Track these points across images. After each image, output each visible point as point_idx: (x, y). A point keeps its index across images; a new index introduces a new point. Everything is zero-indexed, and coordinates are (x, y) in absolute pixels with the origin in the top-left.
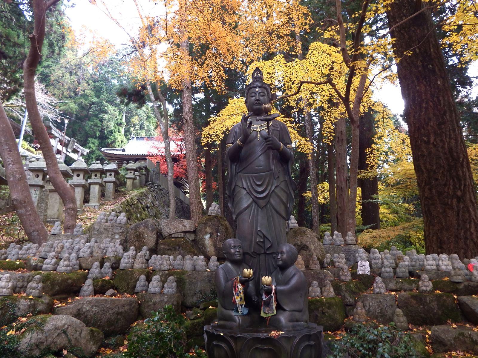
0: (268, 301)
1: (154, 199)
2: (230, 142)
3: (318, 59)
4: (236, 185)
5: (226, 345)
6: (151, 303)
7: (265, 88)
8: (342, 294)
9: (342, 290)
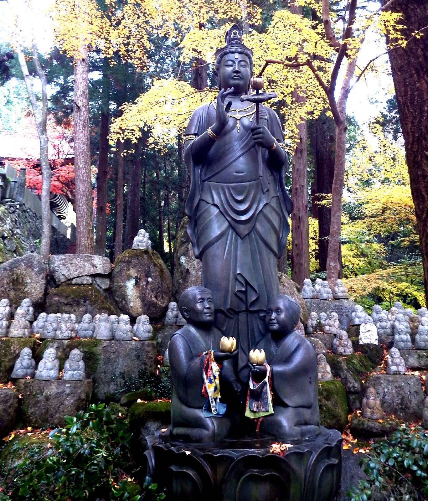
0: (259, 390)
1: (13, 225)
3: (283, 34)
4: (201, 200)
5: (195, 472)
6: (41, 398)
7: (247, 55)
8: (342, 375)
9: (341, 369)
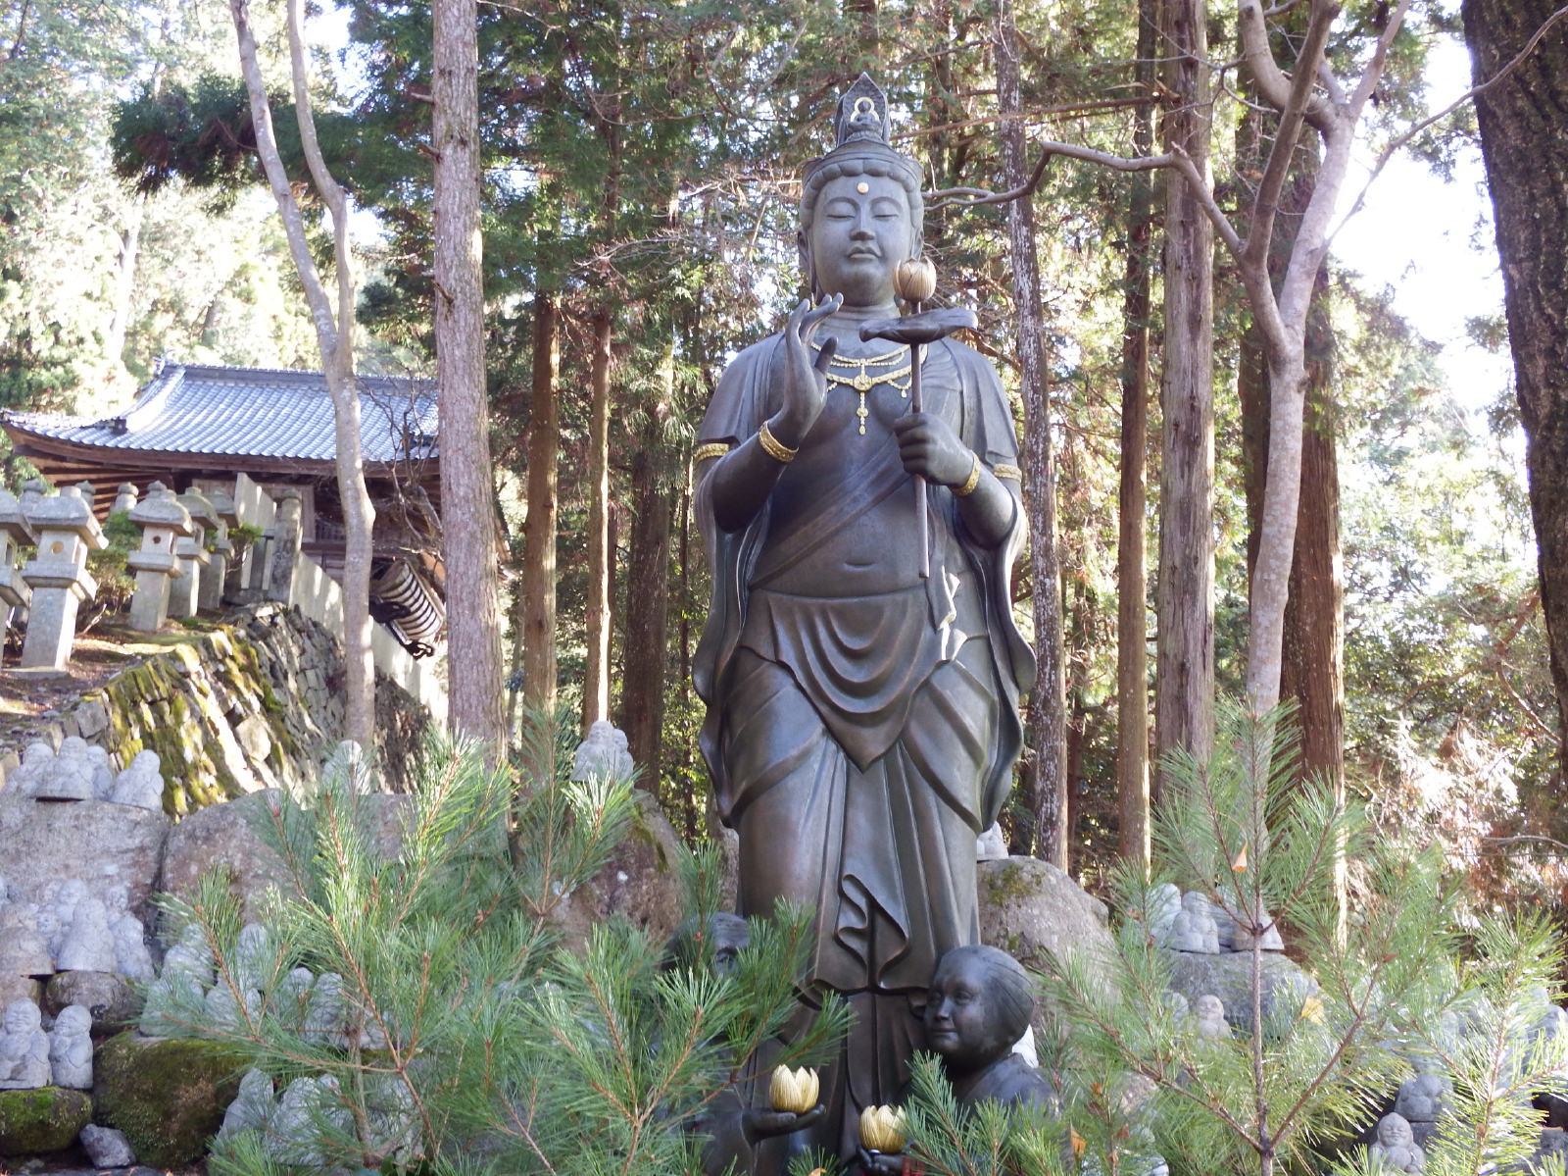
2: (721, 435)
4: (742, 647)
